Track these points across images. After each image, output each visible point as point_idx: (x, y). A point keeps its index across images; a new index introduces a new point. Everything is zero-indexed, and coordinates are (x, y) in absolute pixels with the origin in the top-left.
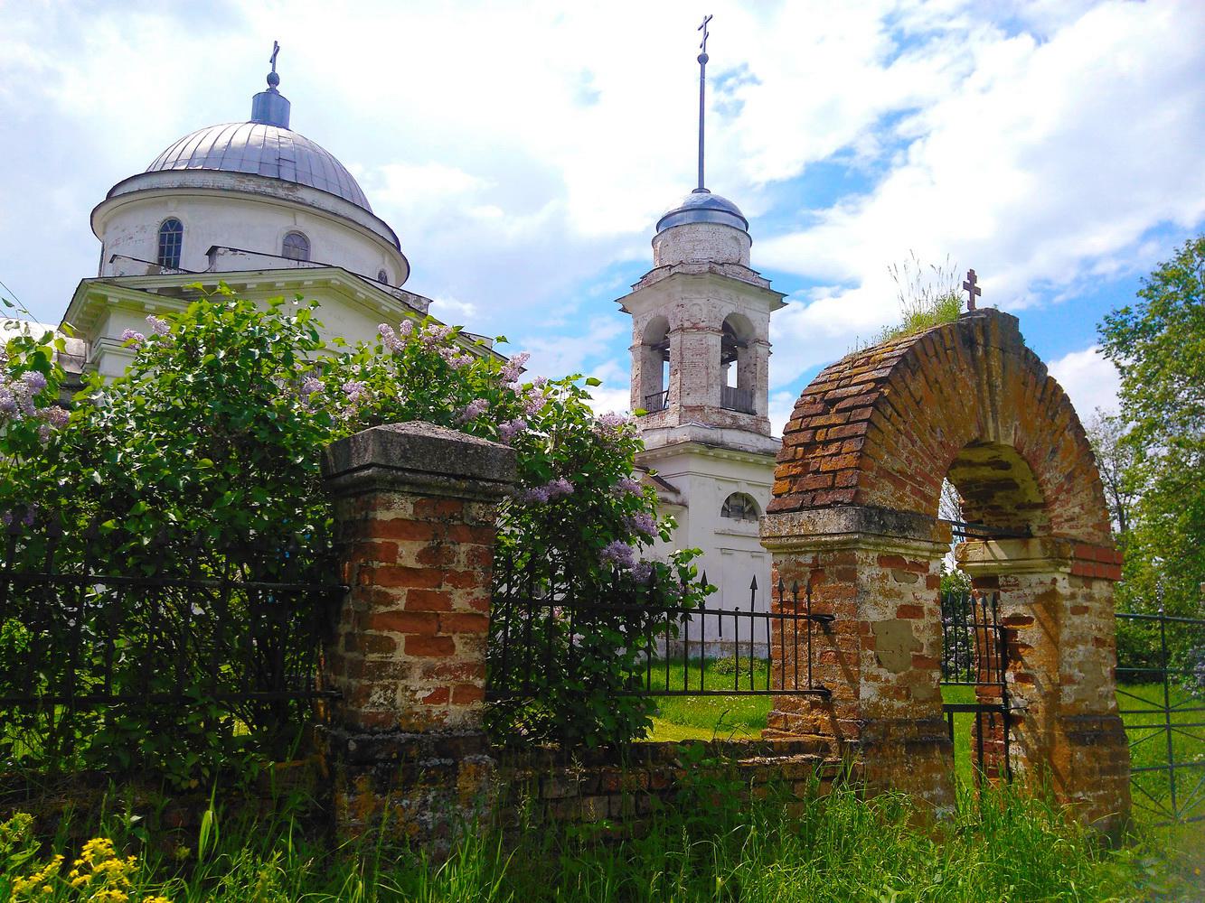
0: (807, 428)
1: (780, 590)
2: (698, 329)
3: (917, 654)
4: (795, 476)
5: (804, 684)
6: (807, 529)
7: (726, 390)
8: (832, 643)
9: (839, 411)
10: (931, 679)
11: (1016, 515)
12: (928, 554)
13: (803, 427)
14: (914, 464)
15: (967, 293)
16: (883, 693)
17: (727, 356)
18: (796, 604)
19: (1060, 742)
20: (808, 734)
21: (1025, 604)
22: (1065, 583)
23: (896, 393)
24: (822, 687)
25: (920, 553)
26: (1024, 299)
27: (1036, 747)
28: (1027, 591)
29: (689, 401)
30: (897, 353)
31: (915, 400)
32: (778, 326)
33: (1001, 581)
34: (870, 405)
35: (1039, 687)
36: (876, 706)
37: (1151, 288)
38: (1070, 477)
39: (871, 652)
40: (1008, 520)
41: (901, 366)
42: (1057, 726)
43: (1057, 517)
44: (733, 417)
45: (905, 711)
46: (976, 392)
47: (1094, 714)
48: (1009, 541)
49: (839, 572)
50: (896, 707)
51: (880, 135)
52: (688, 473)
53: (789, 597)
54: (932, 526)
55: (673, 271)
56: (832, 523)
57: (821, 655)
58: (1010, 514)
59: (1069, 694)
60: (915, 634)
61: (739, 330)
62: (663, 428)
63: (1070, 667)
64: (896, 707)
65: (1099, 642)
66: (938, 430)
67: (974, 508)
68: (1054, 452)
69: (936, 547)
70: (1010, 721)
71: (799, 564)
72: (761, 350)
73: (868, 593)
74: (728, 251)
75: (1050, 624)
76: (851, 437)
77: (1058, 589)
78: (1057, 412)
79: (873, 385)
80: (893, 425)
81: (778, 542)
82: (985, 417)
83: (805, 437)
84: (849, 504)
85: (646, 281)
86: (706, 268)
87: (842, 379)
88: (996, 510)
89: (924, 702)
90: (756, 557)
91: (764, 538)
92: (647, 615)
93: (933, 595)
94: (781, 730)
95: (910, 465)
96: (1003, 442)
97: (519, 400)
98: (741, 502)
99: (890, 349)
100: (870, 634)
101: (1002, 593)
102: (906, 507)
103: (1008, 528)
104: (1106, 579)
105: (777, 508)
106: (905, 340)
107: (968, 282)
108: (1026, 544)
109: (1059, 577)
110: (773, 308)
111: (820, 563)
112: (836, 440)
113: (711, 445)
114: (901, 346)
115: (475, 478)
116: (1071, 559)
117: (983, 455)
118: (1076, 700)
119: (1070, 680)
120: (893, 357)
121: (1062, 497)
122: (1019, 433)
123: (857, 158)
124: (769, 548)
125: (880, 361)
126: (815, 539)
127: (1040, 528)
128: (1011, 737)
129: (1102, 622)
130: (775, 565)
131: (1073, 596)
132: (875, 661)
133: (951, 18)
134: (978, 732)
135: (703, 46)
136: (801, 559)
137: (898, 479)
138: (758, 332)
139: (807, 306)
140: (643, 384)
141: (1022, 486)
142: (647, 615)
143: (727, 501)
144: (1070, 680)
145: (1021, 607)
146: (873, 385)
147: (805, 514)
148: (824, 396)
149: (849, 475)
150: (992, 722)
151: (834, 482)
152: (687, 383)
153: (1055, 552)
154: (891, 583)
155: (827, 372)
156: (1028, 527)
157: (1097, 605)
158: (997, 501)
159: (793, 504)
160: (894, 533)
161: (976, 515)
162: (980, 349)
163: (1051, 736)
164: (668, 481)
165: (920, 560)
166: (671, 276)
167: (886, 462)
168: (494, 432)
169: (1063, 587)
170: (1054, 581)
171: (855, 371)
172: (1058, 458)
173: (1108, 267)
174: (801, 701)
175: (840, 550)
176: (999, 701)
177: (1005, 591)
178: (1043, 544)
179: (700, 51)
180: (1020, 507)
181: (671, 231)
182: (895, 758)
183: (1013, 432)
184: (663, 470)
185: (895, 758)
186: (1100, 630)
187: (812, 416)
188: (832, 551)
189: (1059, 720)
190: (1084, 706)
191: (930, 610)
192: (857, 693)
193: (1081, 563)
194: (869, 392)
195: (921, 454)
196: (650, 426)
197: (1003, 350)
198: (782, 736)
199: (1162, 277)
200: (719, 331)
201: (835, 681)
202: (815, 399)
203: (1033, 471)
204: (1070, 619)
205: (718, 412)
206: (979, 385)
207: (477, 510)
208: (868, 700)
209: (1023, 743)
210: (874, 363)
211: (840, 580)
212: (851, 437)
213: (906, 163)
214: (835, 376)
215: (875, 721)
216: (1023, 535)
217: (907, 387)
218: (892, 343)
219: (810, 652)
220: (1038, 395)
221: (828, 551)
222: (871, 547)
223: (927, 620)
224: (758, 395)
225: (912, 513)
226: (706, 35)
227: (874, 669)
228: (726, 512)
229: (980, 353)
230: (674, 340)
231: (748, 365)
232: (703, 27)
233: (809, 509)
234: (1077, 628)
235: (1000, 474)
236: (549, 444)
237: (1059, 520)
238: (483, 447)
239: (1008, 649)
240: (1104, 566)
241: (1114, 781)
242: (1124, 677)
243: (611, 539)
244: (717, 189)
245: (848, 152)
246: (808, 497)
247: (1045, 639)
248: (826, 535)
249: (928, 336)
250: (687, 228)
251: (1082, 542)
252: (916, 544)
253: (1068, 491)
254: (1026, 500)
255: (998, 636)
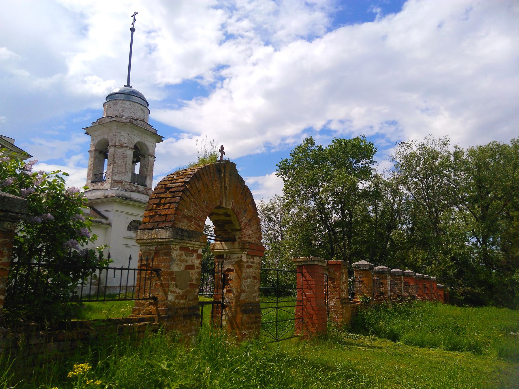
0: (158, 198)
1: (141, 260)
2: (123, 147)
3: (191, 283)
4: (152, 216)
5: (148, 296)
6: (154, 237)
7: (134, 175)
8: (160, 280)
9: (170, 192)
10: (195, 292)
11: (231, 233)
12: (198, 246)
13: (156, 197)
14: (196, 214)
15: (220, 153)
16: (177, 297)
17: (135, 160)
18: (147, 265)
19: (239, 314)
20: (147, 315)
21: (232, 265)
22: (245, 257)
23: (192, 187)
24: (154, 297)
25: (195, 246)
26: (261, 149)
27: (231, 316)
28: (233, 260)
29: (116, 178)
30: (193, 173)
31: (198, 191)
32: (159, 148)
33: (225, 256)
34: (181, 191)
35: (234, 294)
36: (174, 302)
37: (295, 153)
38: (250, 220)
39: (173, 283)
40: (229, 235)
41: (194, 178)
42: (238, 308)
43: (244, 234)
44: (136, 187)
45: (184, 304)
46: (220, 189)
47: (251, 303)
48: (228, 242)
49: (165, 253)
50: (181, 303)
51: (214, 73)
52: (113, 210)
53: (145, 263)
54: (200, 236)
55: (112, 119)
56: (164, 234)
57: (155, 284)
58: (230, 233)
59: (243, 296)
60: (191, 276)
61: (142, 149)
62: (102, 189)
63: (244, 286)
64: (181, 303)
65: (255, 278)
66: (206, 202)
67: (218, 230)
68: (245, 211)
69: (201, 244)
70: (224, 307)
71: (150, 250)
72: (151, 159)
73: (174, 260)
74: (139, 114)
75: (239, 272)
76: (174, 202)
77: (243, 259)
78: (247, 198)
79: (183, 184)
80: (189, 199)
81: (143, 241)
82: (222, 198)
83: (157, 201)
84: (170, 227)
85: (99, 122)
86: (128, 120)
87: (173, 180)
88: (225, 231)
89: (192, 300)
90: (128, 247)
91: (138, 240)
92: (82, 270)
93: (199, 261)
94: (137, 314)
95: (194, 213)
96: (227, 207)
97: (31, 179)
98: (137, 224)
99: (191, 171)
100: (174, 276)
101: (225, 261)
102: (192, 229)
103: (229, 237)
104: (259, 256)
105: (143, 228)
106: (197, 168)
107: (221, 149)
108: (234, 243)
109: (243, 255)
110: (158, 142)
111: (158, 249)
112: (168, 203)
113: (125, 198)
114: (195, 170)
115: (7, 211)
116: (248, 249)
117: (222, 211)
118: (245, 298)
119: (244, 291)
120: (192, 174)
121: (246, 227)
122: (234, 204)
123: (205, 81)
124: (139, 243)
125: (187, 175)
126: (157, 240)
127: (239, 238)
128: (224, 313)
129: (256, 271)
130: (141, 250)
131: (247, 262)
132: (175, 286)
133: (247, 31)
134: (212, 312)
135: (133, 24)
136: (151, 248)
137: (189, 219)
138: (150, 151)
139: (177, 141)
140: (94, 168)
141: (234, 223)
142: (82, 270)
143: (131, 223)
144: (244, 291)
145: (231, 266)
146: (183, 184)
147: (154, 230)
148: (165, 186)
149: (172, 216)
150: (218, 308)
151: (166, 219)
152: (116, 170)
153: (243, 247)
154: (184, 257)
155: (168, 176)
156: (235, 237)
157: (255, 265)
158: (226, 228)
159: (149, 226)
160: (186, 238)
161: (219, 233)
162: (222, 173)
163: (236, 311)
164: (103, 213)
165: (195, 248)
166: (111, 121)
167: (186, 212)
168: (18, 193)
169: (244, 258)
170: (242, 256)
171: (178, 177)
172: (246, 213)
173: (290, 141)
174: (145, 303)
175: (166, 245)
176: (221, 300)
177: (226, 260)
178: (239, 243)
179: (132, 26)
180: (233, 230)
181: (113, 101)
182: (179, 321)
183: (231, 204)
184: (99, 209)
185: (179, 321)
186: (255, 273)
187: (160, 193)
188: (163, 245)
189: (239, 305)
190: (248, 300)
191: (197, 267)
192: (167, 298)
193: (251, 250)
194: (182, 186)
195: (199, 210)
196: (96, 188)
197: (230, 175)
198: (136, 316)
199: (298, 150)
200: (132, 149)
201: (159, 294)
202: (162, 187)
203: (237, 218)
204: (246, 270)
205: (130, 184)
206: (221, 187)
207: (7, 225)
208: (171, 300)
209: (227, 315)
210: (185, 175)
211: (165, 256)
212: (174, 202)
213: (222, 87)
214: (170, 179)
215: (172, 308)
216: (233, 240)
217: (196, 185)
218: (192, 168)
219: (151, 284)
220: (241, 191)
221: (161, 245)
222: (177, 244)
223: (196, 270)
224: (148, 178)
225: (194, 231)
226: (135, 20)
227: (174, 289)
228: (129, 228)
229: (222, 175)
230: (111, 150)
231: (145, 165)
232: (134, 16)
233: (156, 229)
234: (248, 273)
235: (227, 218)
236: (44, 199)
237: (245, 235)
238: (12, 198)
239: (225, 281)
240: (258, 251)
241: (256, 326)
242: (265, 292)
243: (69, 238)
244: (135, 86)
245: (201, 77)
246: (156, 224)
247: (237, 277)
248: (161, 239)
249: (205, 168)
250: (120, 102)
251: (252, 243)
252: (194, 243)
253: (249, 225)
254: (235, 228)
255: (222, 276)
